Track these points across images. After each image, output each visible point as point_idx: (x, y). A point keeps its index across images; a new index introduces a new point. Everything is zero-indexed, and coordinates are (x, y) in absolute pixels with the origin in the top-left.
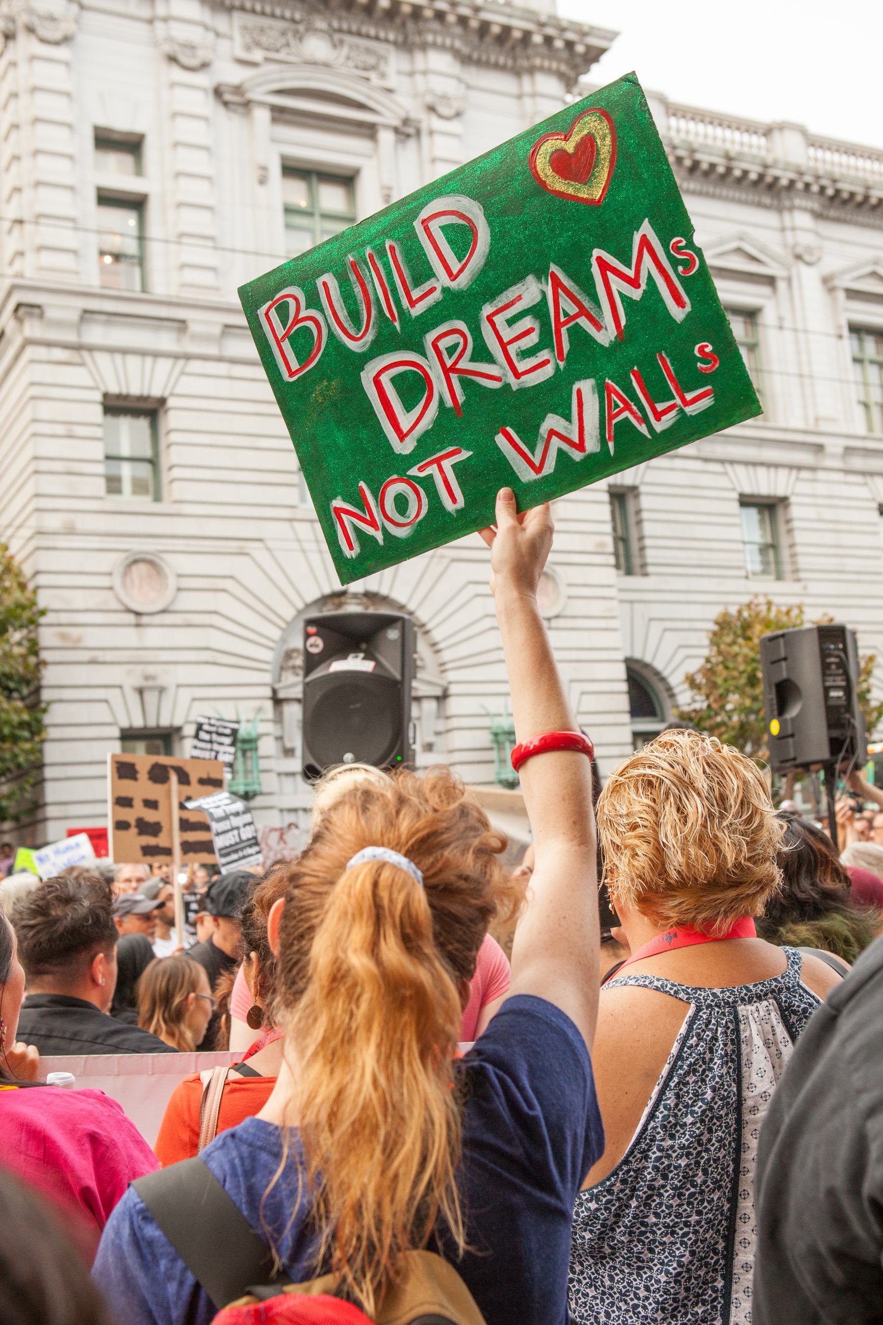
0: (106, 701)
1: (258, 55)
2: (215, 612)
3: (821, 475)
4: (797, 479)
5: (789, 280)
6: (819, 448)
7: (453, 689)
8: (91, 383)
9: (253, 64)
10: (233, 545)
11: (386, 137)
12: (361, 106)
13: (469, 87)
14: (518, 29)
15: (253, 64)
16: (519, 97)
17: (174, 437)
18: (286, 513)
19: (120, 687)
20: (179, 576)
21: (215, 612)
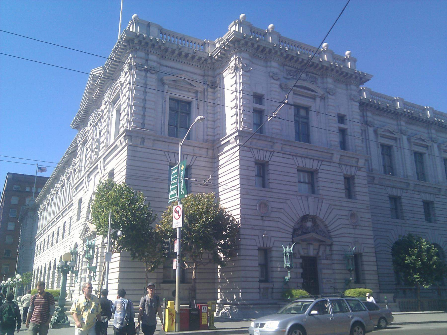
0: (254, 239)
1: (290, 77)
2: (279, 218)
3: (409, 191)
4: (403, 192)
5: (400, 139)
6: (408, 184)
7: (334, 243)
8: (252, 157)
9: (288, 79)
10: (284, 201)
11: (318, 100)
12: (312, 91)
13: (252, 63)
14: (268, 48)
15: (288, 79)
16: (266, 67)
17: (270, 171)
18: (295, 193)
19: (258, 236)
20: (272, 208)
21: (279, 218)
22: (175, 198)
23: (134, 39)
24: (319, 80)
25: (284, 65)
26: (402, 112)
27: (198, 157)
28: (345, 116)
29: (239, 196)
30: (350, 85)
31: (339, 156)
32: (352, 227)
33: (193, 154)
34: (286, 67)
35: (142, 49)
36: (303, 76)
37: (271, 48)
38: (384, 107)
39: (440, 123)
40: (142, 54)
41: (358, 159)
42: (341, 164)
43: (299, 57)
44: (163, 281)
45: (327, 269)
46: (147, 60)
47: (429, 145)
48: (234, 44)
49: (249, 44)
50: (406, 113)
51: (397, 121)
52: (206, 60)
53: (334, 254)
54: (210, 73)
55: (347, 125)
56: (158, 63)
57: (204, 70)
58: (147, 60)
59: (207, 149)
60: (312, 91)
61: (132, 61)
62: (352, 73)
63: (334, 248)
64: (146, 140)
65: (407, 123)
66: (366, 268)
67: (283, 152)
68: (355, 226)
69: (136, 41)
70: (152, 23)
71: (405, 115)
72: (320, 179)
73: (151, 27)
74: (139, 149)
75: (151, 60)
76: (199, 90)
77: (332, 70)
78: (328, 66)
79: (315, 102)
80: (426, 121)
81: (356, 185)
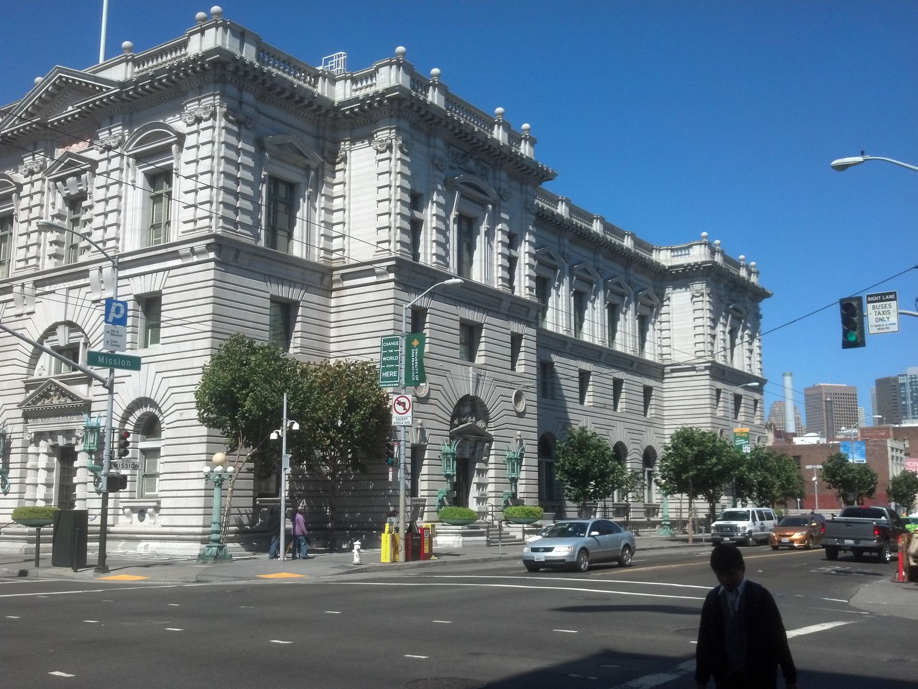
1: (456, 166)
16: (429, 146)
22: (395, 383)
23: (228, 63)
24: (490, 175)
25: (450, 145)
29: (163, 308)
30: (526, 184)
31: (509, 305)
33: (302, 282)
34: (452, 148)
35: (236, 81)
36: (471, 164)
37: (442, 117)
39: (612, 245)
41: (529, 308)
43: (474, 135)
44: (259, 494)
48: (391, 103)
49: (415, 108)
50: (574, 227)
52: (328, 111)
54: (328, 133)
56: (257, 109)
57: (318, 127)
58: (241, 103)
59: (323, 273)
62: (534, 168)
64: (242, 255)
67: (445, 294)
69: (231, 68)
71: (573, 229)
75: (247, 104)
76: (314, 165)
77: (511, 160)
78: (508, 153)
80: (597, 241)
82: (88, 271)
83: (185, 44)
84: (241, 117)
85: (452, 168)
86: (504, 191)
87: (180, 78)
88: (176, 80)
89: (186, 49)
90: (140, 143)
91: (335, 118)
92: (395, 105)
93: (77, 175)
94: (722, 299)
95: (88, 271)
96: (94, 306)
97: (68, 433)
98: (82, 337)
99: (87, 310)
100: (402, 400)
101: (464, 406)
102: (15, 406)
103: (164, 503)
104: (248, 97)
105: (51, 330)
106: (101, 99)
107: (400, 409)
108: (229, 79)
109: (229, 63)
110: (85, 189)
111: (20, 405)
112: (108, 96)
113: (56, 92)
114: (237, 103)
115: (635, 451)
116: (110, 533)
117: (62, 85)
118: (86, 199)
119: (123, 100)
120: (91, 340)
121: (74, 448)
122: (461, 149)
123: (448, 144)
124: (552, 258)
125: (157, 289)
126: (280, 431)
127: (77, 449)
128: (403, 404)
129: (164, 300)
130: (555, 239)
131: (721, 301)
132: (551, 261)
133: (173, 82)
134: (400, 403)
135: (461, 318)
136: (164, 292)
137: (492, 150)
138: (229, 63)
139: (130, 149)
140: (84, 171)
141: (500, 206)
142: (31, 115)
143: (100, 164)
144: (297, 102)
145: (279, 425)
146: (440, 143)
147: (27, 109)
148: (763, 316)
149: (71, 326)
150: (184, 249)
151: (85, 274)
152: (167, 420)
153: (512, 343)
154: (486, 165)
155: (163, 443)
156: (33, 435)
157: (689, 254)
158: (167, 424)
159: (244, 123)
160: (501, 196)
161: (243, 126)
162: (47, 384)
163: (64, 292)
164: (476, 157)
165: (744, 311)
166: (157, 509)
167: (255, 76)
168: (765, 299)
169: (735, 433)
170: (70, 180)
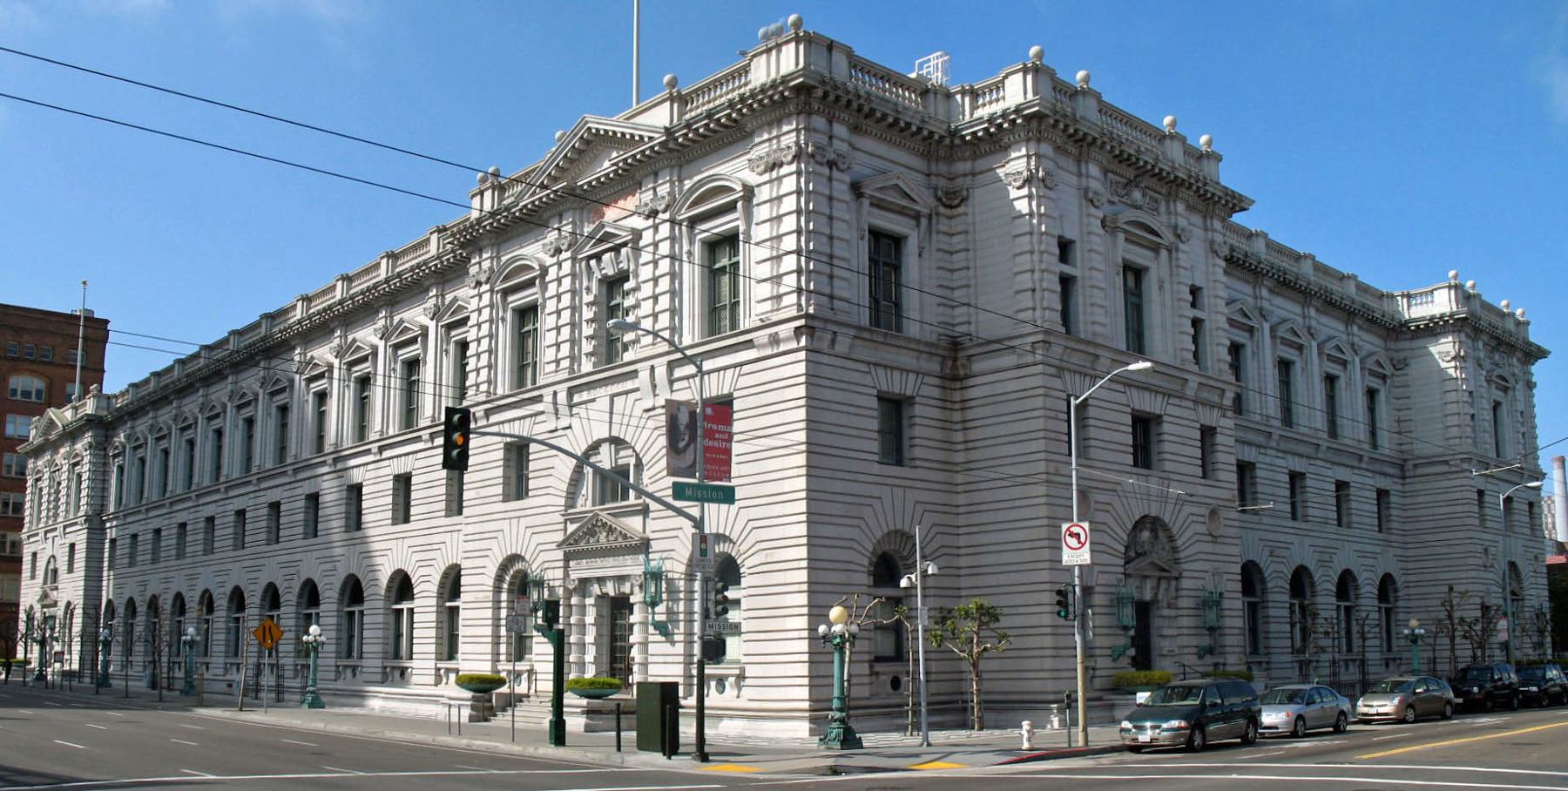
1: (1116, 199)
24: (1163, 208)
26: (942, 133)
27: (926, 378)
28: (1072, 242)
32: (1210, 538)
34: (1110, 175)
36: (1137, 195)
38: (1240, 256)
40: (819, 122)
42: (1063, 369)
45: (1169, 627)
46: (831, 138)
47: (1350, 359)
49: (1061, 126)
51: (1254, 287)
53: (1183, 596)
55: (1075, 266)
58: (831, 138)
60: (1157, 235)
61: (802, 138)
63: (1185, 583)
65: (1271, 291)
66: (1273, 627)
68: (1215, 539)
69: (819, 93)
70: (839, 43)
72: (1166, 437)
73: (834, 52)
74: (825, 359)
79: (1156, 258)
81: (1219, 448)
82: (636, 372)
83: (745, 70)
84: (832, 156)
85: (1112, 203)
86: (1183, 230)
87: (743, 115)
88: (738, 118)
89: (746, 76)
90: (695, 204)
91: (952, 146)
92: (1034, 124)
93: (616, 249)
94: (1482, 362)
95: (636, 372)
96: (646, 415)
97: (621, 579)
98: (632, 456)
99: (1063, 451)
100: (1075, 530)
101: (1141, 531)
102: (554, 546)
103: (749, 671)
104: (840, 130)
105: (594, 447)
106: (643, 152)
107: (1073, 542)
108: (816, 108)
109: (816, 87)
110: (626, 267)
111: (560, 546)
112: (652, 148)
113: (583, 147)
114: (827, 139)
115: (1368, 582)
116: (682, 707)
117: (590, 138)
118: (628, 280)
119: (670, 150)
120: (644, 461)
121: (629, 599)
122: (1122, 176)
123: (1106, 171)
124: (1246, 316)
125: (726, 391)
126: (913, 576)
127: (632, 599)
128: (1078, 536)
129: (737, 405)
130: (1248, 289)
131: (1480, 365)
132: (1245, 321)
133: (735, 121)
134: (1071, 535)
135: (1133, 409)
136: (736, 394)
137: (1164, 174)
138: (816, 87)
139: (683, 211)
140: (625, 244)
141: (1177, 250)
142: (555, 180)
143: (644, 233)
144: (902, 130)
145: (911, 568)
146: (1094, 170)
147: (550, 173)
148: (1538, 385)
149: (617, 442)
150: (761, 336)
151: (634, 374)
152: (748, 563)
153: (1202, 440)
154: (1157, 196)
155: (744, 592)
156: (577, 582)
157: (1432, 302)
158: (749, 568)
159: (836, 164)
160: (1179, 237)
161: (834, 168)
162: (592, 518)
163: (603, 404)
164: (1142, 185)
165: (1512, 380)
166: (741, 677)
167: (849, 102)
168: (1540, 361)
169: (109, 397)
170: (606, 257)
